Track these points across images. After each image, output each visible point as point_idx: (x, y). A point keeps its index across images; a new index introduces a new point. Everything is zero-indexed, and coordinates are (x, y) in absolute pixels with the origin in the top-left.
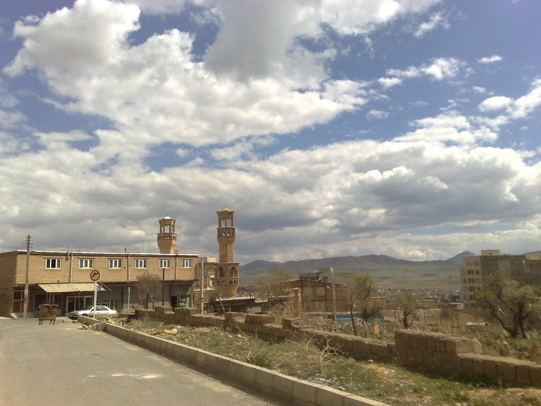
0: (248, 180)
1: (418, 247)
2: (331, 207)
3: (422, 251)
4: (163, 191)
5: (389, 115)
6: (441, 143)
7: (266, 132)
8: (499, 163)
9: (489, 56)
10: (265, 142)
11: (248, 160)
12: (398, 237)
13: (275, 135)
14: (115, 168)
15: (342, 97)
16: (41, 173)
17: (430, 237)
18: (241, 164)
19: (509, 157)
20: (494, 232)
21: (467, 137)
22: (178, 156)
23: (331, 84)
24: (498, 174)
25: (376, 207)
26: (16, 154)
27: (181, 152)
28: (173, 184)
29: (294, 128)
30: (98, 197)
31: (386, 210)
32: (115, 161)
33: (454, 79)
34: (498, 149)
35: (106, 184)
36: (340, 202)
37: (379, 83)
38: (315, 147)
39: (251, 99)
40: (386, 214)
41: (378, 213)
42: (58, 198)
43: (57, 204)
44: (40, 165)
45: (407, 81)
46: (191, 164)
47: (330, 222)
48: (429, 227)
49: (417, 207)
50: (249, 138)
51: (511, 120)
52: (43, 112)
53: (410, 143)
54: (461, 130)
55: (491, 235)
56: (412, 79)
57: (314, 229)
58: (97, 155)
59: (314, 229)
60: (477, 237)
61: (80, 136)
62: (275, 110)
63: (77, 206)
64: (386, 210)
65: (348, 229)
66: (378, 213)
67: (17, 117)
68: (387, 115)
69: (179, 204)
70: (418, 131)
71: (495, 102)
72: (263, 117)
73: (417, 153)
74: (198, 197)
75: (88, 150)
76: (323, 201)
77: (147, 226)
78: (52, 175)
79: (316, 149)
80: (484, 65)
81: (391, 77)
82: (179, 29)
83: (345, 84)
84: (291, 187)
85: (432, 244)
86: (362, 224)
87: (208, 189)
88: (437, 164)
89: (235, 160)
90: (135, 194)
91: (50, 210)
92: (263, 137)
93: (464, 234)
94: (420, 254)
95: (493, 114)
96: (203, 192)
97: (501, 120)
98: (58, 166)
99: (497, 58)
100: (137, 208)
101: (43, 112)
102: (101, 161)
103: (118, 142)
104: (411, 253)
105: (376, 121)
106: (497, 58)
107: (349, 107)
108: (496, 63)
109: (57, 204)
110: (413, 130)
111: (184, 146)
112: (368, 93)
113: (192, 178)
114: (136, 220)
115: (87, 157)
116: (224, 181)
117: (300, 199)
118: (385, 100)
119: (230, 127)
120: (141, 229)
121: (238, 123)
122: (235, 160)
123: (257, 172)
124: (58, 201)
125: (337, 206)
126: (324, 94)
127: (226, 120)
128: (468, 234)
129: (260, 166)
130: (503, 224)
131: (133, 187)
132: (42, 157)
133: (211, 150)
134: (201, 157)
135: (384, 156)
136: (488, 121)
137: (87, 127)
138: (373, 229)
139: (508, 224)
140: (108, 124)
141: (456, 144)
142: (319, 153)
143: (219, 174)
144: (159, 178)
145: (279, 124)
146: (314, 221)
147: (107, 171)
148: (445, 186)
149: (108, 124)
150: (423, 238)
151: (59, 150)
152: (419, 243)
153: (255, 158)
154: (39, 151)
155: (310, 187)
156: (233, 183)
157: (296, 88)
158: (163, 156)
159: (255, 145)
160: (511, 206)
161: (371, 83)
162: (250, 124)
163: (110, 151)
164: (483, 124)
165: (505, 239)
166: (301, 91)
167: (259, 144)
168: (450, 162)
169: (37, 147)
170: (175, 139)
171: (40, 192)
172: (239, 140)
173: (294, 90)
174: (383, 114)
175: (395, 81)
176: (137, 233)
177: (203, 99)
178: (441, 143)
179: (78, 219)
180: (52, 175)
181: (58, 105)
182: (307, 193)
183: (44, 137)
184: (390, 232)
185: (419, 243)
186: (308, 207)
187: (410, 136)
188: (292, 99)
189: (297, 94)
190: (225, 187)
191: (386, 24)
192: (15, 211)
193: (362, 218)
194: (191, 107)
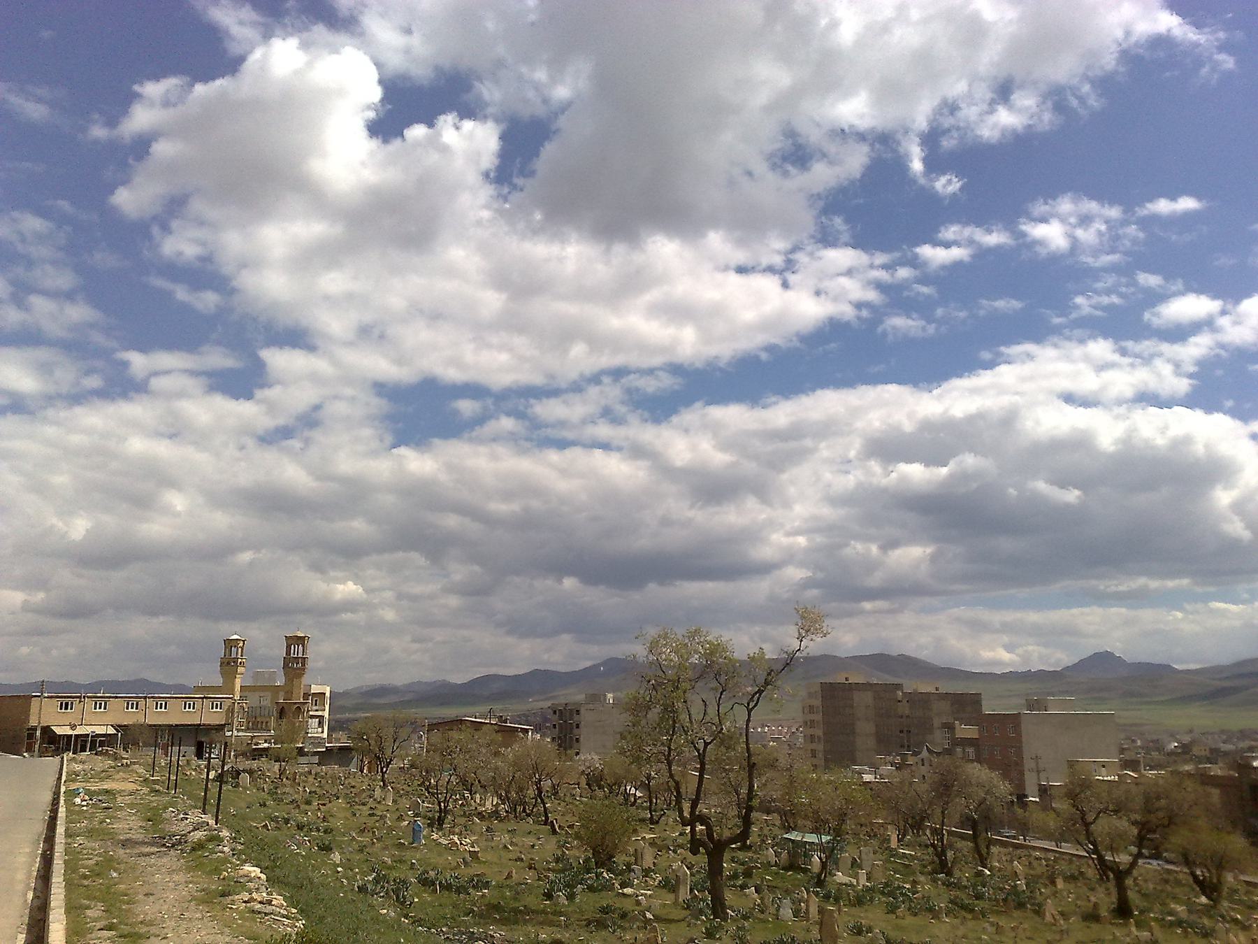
0: (617, 469)
1: (1005, 639)
2: (802, 540)
3: (1009, 648)
4: (421, 495)
5: (936, 329)
6: (1062, 399)
7: (657, 361)
8: (1199, 449)
9: (1173, 198)
10: (650, 385)
11: (620, 424)
12: (956, 611)
13: (676, 369)
14: (316, 434)
15: (834, 285)
16: (137, 445)
17: (1033, 617)
18: (604, 431)
19: (1213, 432)
20: (1188, 607)
21: (1124, 380)
22: (456, 413)
23: (811, 254)
24: (1193, 474)
25: (912, 540)
26: (77, 398)
27: (466, 407)
28: (443, 477)
29: (724, 350)
30: (271, 502)
31: (929, 550)
32: (310, 420)
33: (1096, 252)
34: (1198, 414)
35: (290, 472)
36: (829, 528)
37: (916, 256)
38: (773, 399)
39: (629, 286)
40: (934, 558)
41: (913, 556)
42: (178, 501)
43: (178, 515)
44: (136, 426)
45: (983, 254)
46: (478, 431)
47: (795, 574)
48: (1023, 593)
49: (1006, 544)
50: (618, 373)
51: (1222, 346)
52: (154, 305)
53: (593, 391)
54: (1102, 367)
55: (1179, 615)
56: (997, 250)
57: (760, 589)
58: (272, 408)
59: (760, 589)
60: (1147, 616)
61: (218, 359)
62: (676, 312)
63: (221, 521)
64: (929, 550)
65: (843, 587)
66: (913, 556)
67: (78, 313)
68: (931, 329)
69: (452, 521)
70: (1003, 368)
71: (1189, 306)
72: (654, 331)
73: (1009, 420)
74: (499, 507)
75: (249, 396)
76: (788, 524)
77: (371, 572)
78: (163, 450)
79: (775, 403)
80: (1155, 219)
81: (947, 245)
82: (419, 121)
83: (841, 257)
84: (713, 489)
85: (1037, 632)
86: (876, 580)
87: (528, 489)
88: (1057, 446)
89: (590, 420)
90: (353, 495)
91: (155, 529)
92: (650, 372)
93: (1114, 610)
94: (1005, 656)
95: (1180, 333)
96: (508, 495)
97: (1198, 347)
98: (175, 431)
99: (1187, 204)
100: (358, 527)
101: (154, 305)
102: (281, 421)
103: (315, 378)
104: (987, 654)
105: (908, 343)
106: (1187, 204)
107: (846, 311)
108: (1187, 216)
109: (178, 516)
110: (990, 365)
111: (473, 390)
112: (892, 275)
113: (482, 464)
114: (349, 554)
115: (245, 409)
116: (564, 473)
117: (731, 517)
118: (928, 297)
119: (578, 350)
120: (357, 579)
121: (596, 342)
122: (590, 420)
123: (637, 452)
124: (179, 508)
125: (819, 539)
126: (792, 278)
127: (565, 335)
128: (1123, 610)
129: (649, 434)
130: (1199, 590)
131: (346, 481)
132: (133, 409)
133: (532, 401)
134: (508, 414)
135: (928, 426)
136: (1165, 347)
137: (239, 342)
138: (900, 591)
139: (1211, 589)
140: (297, 337)
141: (1069, 398)
142: (782, 413)
143: (554, 456)
144: (419, 464)
145: (687, 342)
146: (765, 569)
147: (296, 444)
148: (1072, 496)
149: (297, 337)
150: (1009, 616)
151: (181, 394)
152: (1006, 628)
153: (633, 419)
154: (132, 394)
155: (761, 491)
156: (600, 473)
157: (733, 264)
158: (421, 410)
159: (629, 391)
160: (1231, 547)
161: (897, 255)
162: (615, 342)
163: (299, 398)
164: (1160, 355)
165: (1199, 626)
166: (741, 270)
167: (637, 390)
168: (1080, 443)
169: (122, 386)
170: (452, 375)
171: (139, 489)
172: (595, 379)
173: (726, 268)
174: (924, 329)
175: (956, 253)
176: (347, 589)
177: (521, 285)
178: (1062, 399)
179: (220, 551)
180: (163, 450)
181: (182, 294)
182: (751, 503)
183: (138, 362)
184: (927, 600)
185: (1006, 628)
186: (753, 535)
187: (984, 378)
188: (716, 289)
189: (733, 278)
190: (563, 486)
191: (278, 31)
192: (79, 528)
193: (871, 566)
194: (492, 301)
